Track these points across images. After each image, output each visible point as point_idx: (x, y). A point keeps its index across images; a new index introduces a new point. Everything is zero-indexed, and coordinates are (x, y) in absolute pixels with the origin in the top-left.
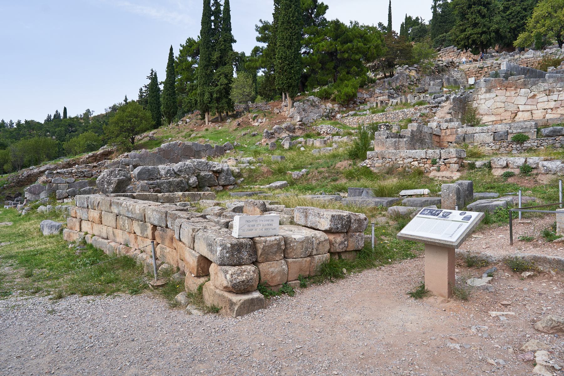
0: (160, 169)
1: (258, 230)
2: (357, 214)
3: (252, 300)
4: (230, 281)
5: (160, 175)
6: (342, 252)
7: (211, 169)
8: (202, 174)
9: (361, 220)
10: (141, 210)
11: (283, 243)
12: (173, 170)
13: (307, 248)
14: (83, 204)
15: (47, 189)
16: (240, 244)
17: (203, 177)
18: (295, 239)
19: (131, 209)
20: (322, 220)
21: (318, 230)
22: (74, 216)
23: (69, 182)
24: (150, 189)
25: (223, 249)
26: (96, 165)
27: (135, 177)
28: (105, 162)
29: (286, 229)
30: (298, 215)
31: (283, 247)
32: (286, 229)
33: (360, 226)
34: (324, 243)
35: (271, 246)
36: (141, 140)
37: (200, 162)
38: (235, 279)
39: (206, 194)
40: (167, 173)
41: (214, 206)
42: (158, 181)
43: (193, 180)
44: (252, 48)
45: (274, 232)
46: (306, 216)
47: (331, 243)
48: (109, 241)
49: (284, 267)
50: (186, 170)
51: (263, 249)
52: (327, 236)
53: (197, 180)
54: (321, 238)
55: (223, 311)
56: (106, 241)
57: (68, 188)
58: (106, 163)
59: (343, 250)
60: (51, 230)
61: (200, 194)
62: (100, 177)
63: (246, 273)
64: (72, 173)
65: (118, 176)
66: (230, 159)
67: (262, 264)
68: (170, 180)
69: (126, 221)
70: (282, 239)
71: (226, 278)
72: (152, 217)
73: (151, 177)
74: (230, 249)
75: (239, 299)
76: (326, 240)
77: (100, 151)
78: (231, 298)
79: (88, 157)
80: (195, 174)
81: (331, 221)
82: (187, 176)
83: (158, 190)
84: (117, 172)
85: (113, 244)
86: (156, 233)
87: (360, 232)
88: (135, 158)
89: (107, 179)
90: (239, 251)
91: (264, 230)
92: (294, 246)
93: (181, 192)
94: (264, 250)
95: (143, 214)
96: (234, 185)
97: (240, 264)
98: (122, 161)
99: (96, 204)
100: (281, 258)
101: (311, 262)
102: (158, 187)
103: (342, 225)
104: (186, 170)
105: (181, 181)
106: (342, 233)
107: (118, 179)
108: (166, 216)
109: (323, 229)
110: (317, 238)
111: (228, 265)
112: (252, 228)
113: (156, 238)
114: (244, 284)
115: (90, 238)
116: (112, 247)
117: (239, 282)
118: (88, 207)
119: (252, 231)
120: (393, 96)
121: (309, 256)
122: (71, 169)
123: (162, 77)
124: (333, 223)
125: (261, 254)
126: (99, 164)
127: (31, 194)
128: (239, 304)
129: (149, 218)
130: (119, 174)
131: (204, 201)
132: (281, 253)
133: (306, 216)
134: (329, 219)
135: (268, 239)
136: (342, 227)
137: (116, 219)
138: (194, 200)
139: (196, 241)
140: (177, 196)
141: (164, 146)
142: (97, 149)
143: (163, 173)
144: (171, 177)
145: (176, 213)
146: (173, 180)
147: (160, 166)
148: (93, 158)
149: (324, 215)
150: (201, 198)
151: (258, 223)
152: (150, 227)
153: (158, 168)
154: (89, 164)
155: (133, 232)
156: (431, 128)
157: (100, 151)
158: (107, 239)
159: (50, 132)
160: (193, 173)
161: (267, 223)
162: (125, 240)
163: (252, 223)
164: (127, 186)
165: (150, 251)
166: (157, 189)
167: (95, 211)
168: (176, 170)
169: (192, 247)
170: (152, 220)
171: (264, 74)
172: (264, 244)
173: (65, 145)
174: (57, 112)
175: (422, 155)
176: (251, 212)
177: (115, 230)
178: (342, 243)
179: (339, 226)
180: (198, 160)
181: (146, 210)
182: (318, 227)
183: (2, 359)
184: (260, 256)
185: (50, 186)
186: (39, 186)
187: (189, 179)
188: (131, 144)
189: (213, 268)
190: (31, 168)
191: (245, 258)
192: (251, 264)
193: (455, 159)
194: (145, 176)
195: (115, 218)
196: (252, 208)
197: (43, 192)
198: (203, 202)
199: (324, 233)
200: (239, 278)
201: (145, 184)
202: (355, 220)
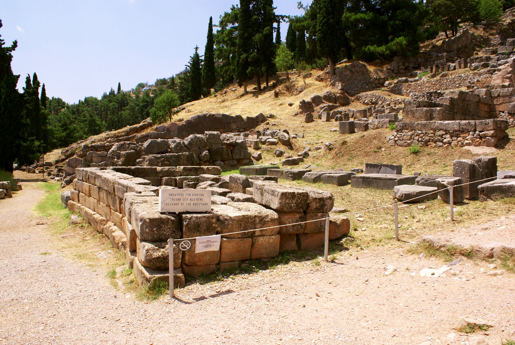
0: (170, 142)
1: (185, 204)
90: (159, 227)
91: (192, 204)
112: (177, 202)
120: (452, 59)
123: (202, 52)
127: (69, 167)
147: (170, 140)
151: (184, 197)
156: (478, 96)
161: (195, 197)
175: (455, 126)
185: (86, 160)
193: (492, 132)
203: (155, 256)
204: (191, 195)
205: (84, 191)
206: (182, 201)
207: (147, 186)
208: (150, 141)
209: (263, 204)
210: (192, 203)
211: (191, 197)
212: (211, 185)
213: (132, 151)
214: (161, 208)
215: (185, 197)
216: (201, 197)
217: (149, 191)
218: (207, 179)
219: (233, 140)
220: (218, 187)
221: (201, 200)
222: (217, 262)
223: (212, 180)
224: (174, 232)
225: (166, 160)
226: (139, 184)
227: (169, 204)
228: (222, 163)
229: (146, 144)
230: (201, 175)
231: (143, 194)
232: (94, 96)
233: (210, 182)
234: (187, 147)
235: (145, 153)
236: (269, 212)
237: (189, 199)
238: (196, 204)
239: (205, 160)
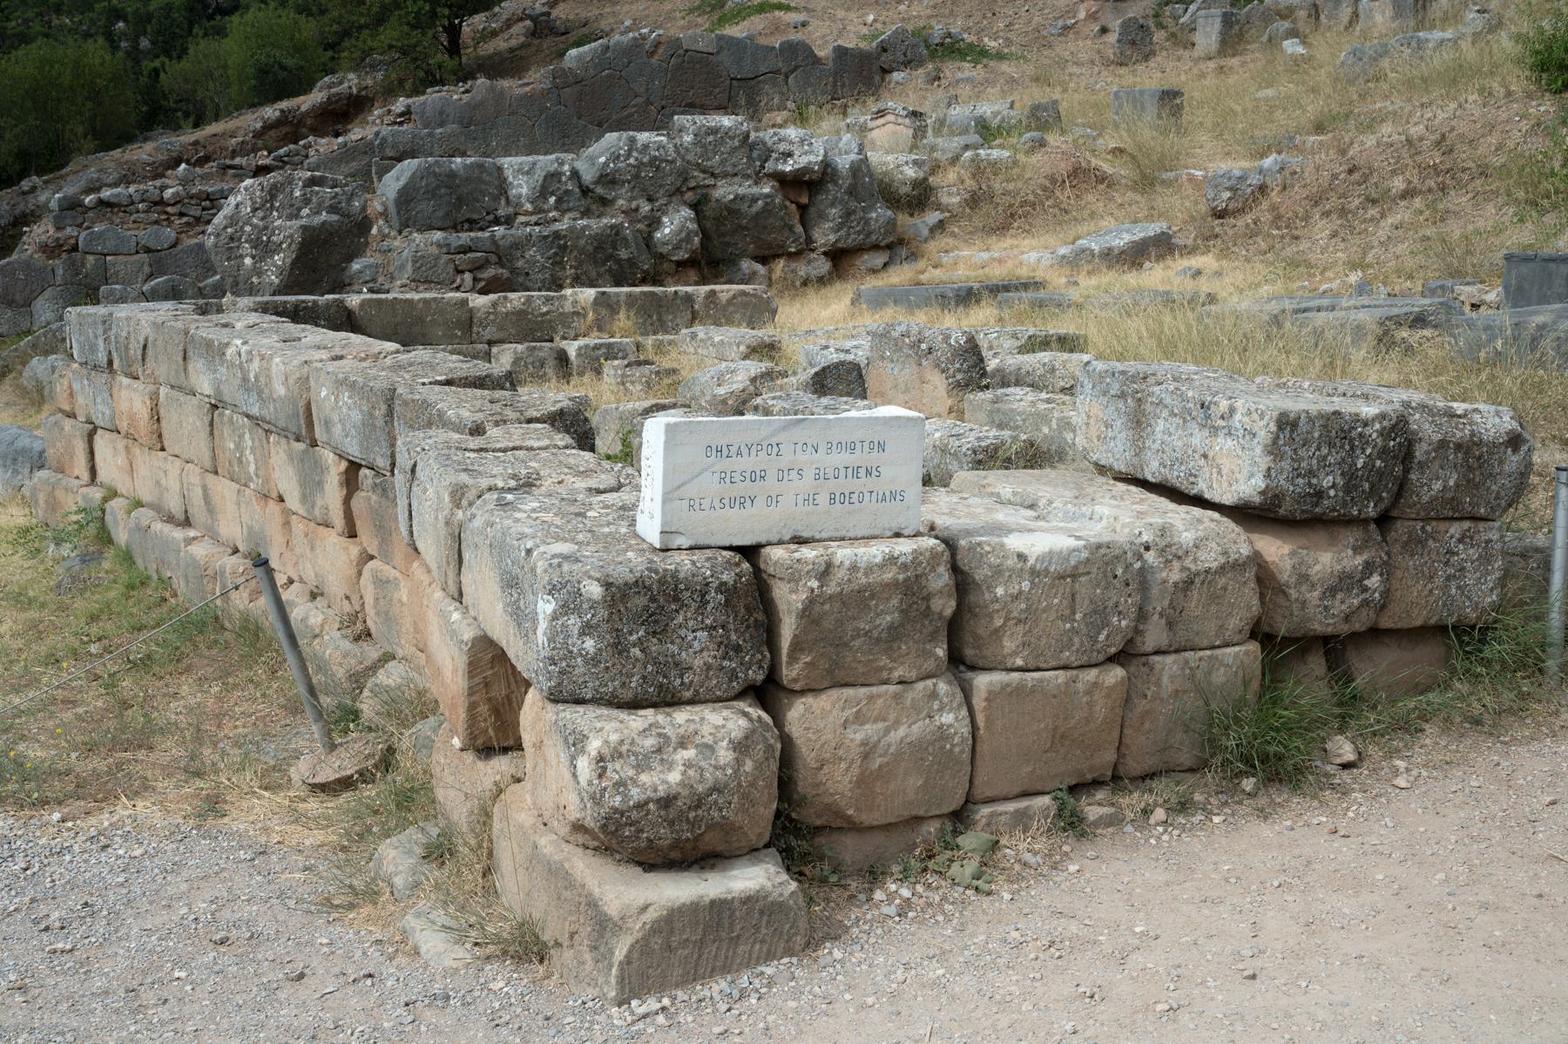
1: (787, 502)
2: (1460, 408)
3: (719, 907)
4: (593, 798)
5: (508, 202)
6: (1354, 637)
7: (770, 166)
8: (725, 191)
9: (1480, 443)
10: (291, 381)
11: (941, 579)
12: (575, 174)
13: (1099, 617)
14: (93, 349)
15: (59, 280)
16: (662, 581)
17: (731, 210)
18: (1021, 557)
19: (256, 377)
20: (1224, 444)
21: (1199, 501)
22: (67, 408)
23: (152, 244)
24: (460, 272)
25: (565, 609)
26: (268, 161)
27: (384, 214)
28: (306, 147)
29: (1006, 491)
30: (1096, 410)
31: (946, 606)
32: (1006, 491)
33: (1468, 484)
34: (1222, 582)
35: (860, 598)
36: (494, 34)
37: (714, 131)
38: (620, 784)
39: (724, 297)
40: (543, 192)
41: (745, 357)
42: (499, 230)
43: (674, 224)
45: (891, 516)
46: (1138, 422)
47: (1265, 577)
48: (192, 533)
49: (947, 718)
50: (637, 176)
51: (808, 613)
52: (1241, 541)
53: (693, 226)
54: (1202, 555)
55: (564, 958)
56: (178, 534)
57: (150, 276)
58: (312, 152)
59: (1358, 626)
60: (16, 472)
61: (689, 298)
62: (219, 219)
63: (690, 753)
64: (161, 202)
65: (305, 211)
66: (881, 113)
67: (809, 700)
68: (557, 226)
69: (247, 436)
70: (934, 556)
71: (575, 775)
72: (336, 418)
73: (465, 213)
74: (603, 613)
75: (641, 902)
76: (1232, 567)
77: (307, 102)
78: (596, 891)
79: (259, 125)
80: (689, 196)
81: (1273, 449)
82: (646, 208)
83: (495, 279)
84: (297, 193)
85: (200, 551)
86: (358, 502)
87: (1475, 518)
88: (441, 125)
89: (254, 227)
91: (823, 499)
92: (1017, 597)
93: (592, 285)
94: (816, 622)
95: (302, 403)
96: (889, 247)
97: (667, 700)
98: (384, 140)
99: (135, 350)
100: (930, 665)
101: (1128, 697)
102: (500, 263)
103: (1351, 477)
105: (616, 229)
106: (1348, 522)
107: (304, 228)
108: (390, 413)
109: (1228, 499)
110: (1170, 552)
111: (597, 701)
113: (358, 524)
114: (672, 813)
115: (121, 515)
116: (193, 562)
117: (640, 806)
118: (110, 363)
119: (749, 510)
121: (1123, 656)
122: (158, 183)
124: (1286, 465)
125: (796, 646)
126: (279, 159)
128: (636, 928)
129: (328, 424)
130: (306, 201)
131: (701, 335)
132: (933, 637)
133: (1138, 422)
134: (1264, 435)
135: (843, 554)
136: (1348, 489)
137: (211, 424)
138: (661, 327)
139: (466, 556)
140: (568, 308)
141: (580, 58)
142: (305, 87)
144: (564, 212)
145: (432, 398)
146: (571, 229)
148: (285, 130)
149: (1232, 410)
150: (694, 318)
152: (334, 470)
153: (500, 169)
154: (237, 161)
155: (274, 495)
157: (307, 102)
158: (187, 522)
159: (126, 21)
160: (678, 191)
161: (842, 459)
162: (250, 528)
163: (746, 463)
164: (350, 258)
165: (341, 594)
166: (490, 272)
167: (135, 384)
168: (588, 176)
169: (453, 589)
170: (337, 430)
172: (814, 584)
173: (174, 73)
176: (907, 390)
177: (210, 478)
178: (1345, 582)
179: (1327, 481)
181: (312, 383)
182: (1202, 487)
184: (793, 658)
185: (74, 268)
186: (27, 265)
187: (654, 223)
188: (442, 57)
189: (534, 714)
190: (25, 184)
191: (698, 663)
192: (740, 696)
195: (207, 420)
196: (910, 370)
197: (47, 294)
198: (694, 336)
199: (1228, 524)
200: (644, 778)
201: (434, 250)
202: (1443, 444)
205: (123, 426)
208: (409, 166)
209: (1150, 478)
214: (664, 524)
216: (874, 458)
219: (812, 158)
221: (868, 472)
222: (955, 803)
229: (392, 183)
234: (591, 197)
236: (1184, 523)
238: (846, 498)
239: (682, 255)
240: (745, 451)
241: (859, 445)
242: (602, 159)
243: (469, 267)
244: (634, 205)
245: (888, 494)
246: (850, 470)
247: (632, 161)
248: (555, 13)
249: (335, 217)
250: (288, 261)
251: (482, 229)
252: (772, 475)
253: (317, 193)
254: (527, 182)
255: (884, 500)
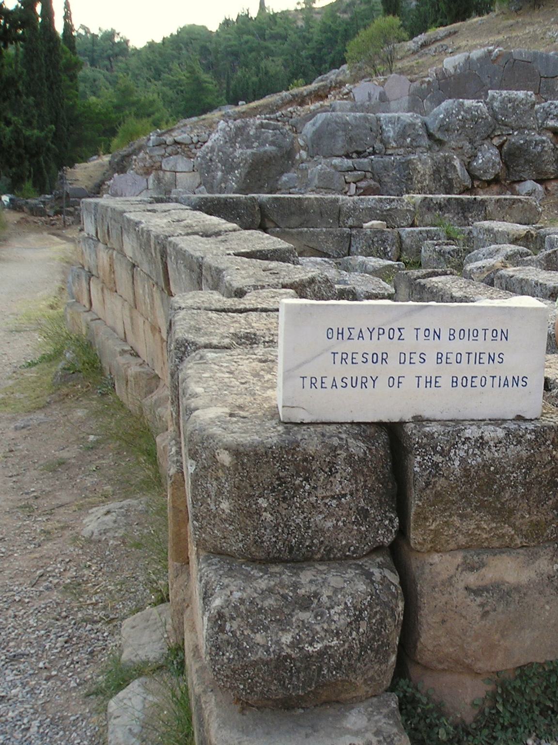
1: (409, 382)
12: (425, 125)
44: (221, 21)
50: (463, 127)
91: (445, 382)
104: (463, 127)
112: (369, 369)
143: (391, 134)
166: (363, 184)
168: (433, 128)
171: (15, 191)
174: (3, 2)
180: (504, 93)
183: (374, 740)
194: (340, 144)
203: (261, 654)
204: (445, 335)
206: (393, 367)
207: (273, 264)
210: (446, 374)
211: (445, 345)
212: (511, 258)
213: (268, 147)
215: (409, 342)
216: (496, 347)
217: (275, 286)
218: (495, 237)
220: (538, 264)
221: (491, 358)
223: (515, 241)
224: (363, 512)
225: (369, 175)
226: (249, 255)
227: (328, 382)
228: (539, 187)
230: (477, 223)
231: (248, 301)
232: (199, 23)
233: (510, 248)
235: (308, 155)
237: (431, 358)
238: (467, 382)
240: (366, 334)
241: (481, 333)
242: (442, 116)
243: (353, 180)
244: (460, 145)
245: (510, 379)
246: (472, 357)
247: (460, 117)
248: (471, 55)
249: (274, 148)
250: (243, 174)
251: (365, 157)
252: (393, 360)
253: (264, 133)
254: (393, 129)
255: (506, 384)
